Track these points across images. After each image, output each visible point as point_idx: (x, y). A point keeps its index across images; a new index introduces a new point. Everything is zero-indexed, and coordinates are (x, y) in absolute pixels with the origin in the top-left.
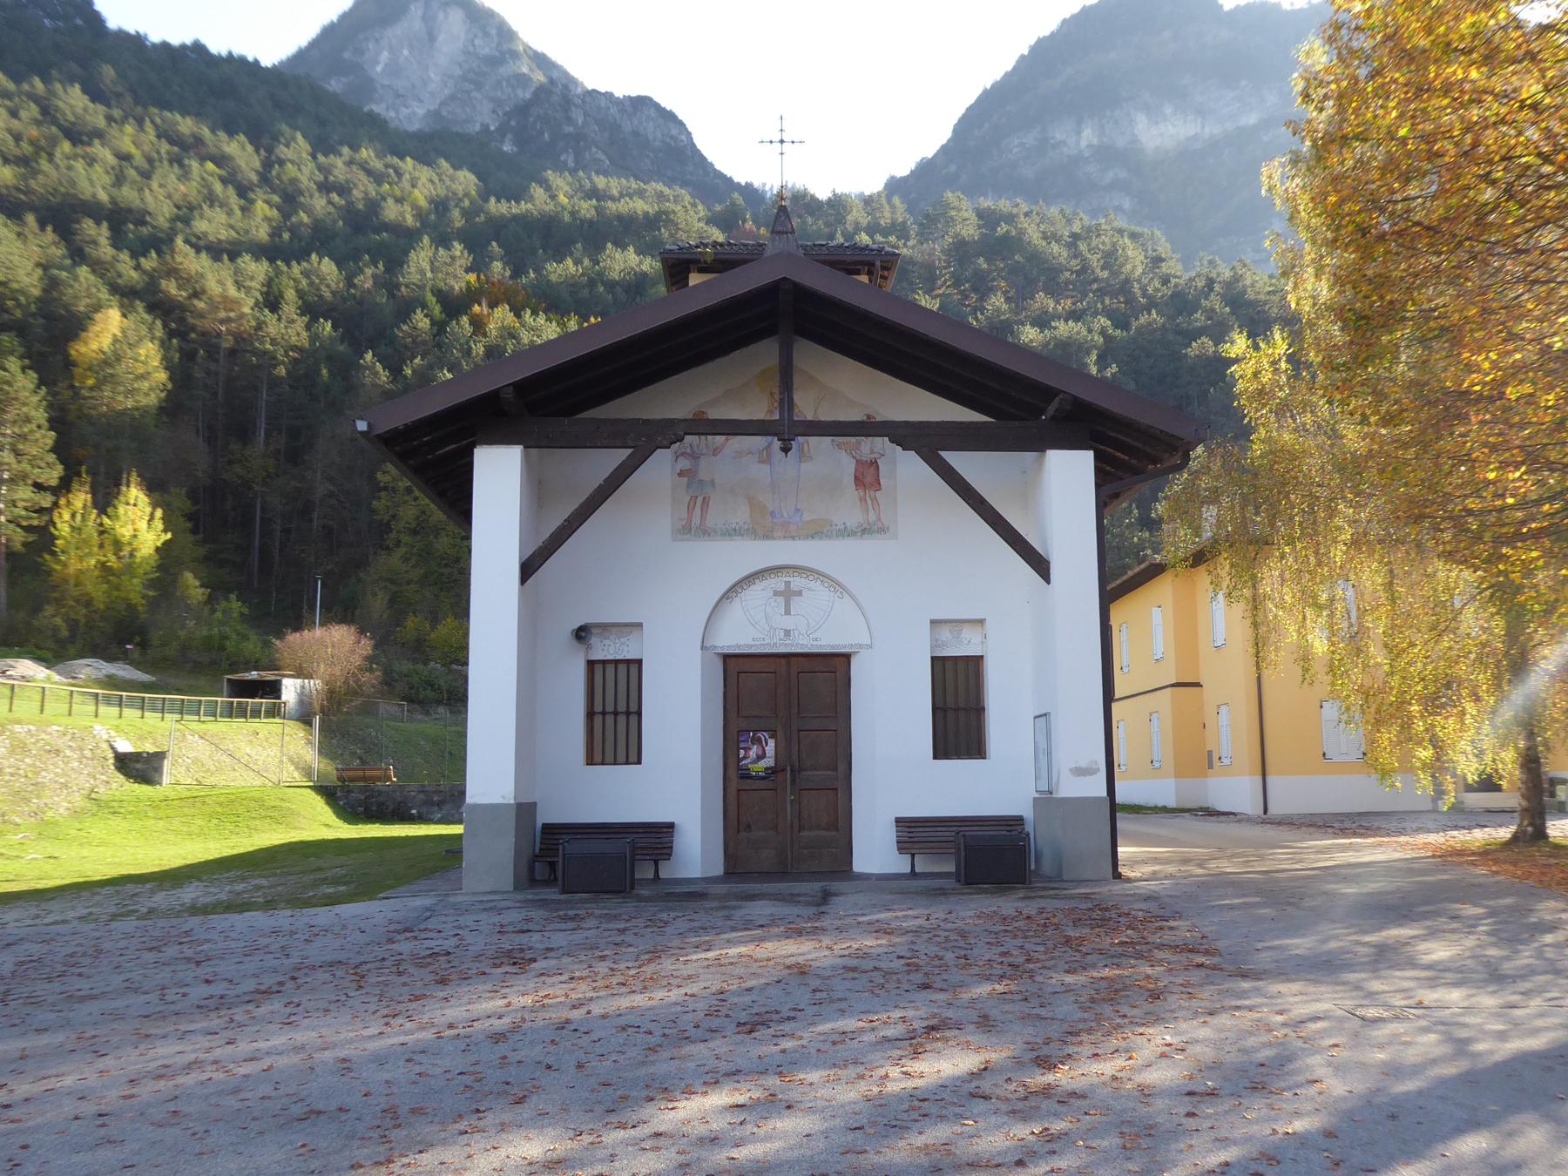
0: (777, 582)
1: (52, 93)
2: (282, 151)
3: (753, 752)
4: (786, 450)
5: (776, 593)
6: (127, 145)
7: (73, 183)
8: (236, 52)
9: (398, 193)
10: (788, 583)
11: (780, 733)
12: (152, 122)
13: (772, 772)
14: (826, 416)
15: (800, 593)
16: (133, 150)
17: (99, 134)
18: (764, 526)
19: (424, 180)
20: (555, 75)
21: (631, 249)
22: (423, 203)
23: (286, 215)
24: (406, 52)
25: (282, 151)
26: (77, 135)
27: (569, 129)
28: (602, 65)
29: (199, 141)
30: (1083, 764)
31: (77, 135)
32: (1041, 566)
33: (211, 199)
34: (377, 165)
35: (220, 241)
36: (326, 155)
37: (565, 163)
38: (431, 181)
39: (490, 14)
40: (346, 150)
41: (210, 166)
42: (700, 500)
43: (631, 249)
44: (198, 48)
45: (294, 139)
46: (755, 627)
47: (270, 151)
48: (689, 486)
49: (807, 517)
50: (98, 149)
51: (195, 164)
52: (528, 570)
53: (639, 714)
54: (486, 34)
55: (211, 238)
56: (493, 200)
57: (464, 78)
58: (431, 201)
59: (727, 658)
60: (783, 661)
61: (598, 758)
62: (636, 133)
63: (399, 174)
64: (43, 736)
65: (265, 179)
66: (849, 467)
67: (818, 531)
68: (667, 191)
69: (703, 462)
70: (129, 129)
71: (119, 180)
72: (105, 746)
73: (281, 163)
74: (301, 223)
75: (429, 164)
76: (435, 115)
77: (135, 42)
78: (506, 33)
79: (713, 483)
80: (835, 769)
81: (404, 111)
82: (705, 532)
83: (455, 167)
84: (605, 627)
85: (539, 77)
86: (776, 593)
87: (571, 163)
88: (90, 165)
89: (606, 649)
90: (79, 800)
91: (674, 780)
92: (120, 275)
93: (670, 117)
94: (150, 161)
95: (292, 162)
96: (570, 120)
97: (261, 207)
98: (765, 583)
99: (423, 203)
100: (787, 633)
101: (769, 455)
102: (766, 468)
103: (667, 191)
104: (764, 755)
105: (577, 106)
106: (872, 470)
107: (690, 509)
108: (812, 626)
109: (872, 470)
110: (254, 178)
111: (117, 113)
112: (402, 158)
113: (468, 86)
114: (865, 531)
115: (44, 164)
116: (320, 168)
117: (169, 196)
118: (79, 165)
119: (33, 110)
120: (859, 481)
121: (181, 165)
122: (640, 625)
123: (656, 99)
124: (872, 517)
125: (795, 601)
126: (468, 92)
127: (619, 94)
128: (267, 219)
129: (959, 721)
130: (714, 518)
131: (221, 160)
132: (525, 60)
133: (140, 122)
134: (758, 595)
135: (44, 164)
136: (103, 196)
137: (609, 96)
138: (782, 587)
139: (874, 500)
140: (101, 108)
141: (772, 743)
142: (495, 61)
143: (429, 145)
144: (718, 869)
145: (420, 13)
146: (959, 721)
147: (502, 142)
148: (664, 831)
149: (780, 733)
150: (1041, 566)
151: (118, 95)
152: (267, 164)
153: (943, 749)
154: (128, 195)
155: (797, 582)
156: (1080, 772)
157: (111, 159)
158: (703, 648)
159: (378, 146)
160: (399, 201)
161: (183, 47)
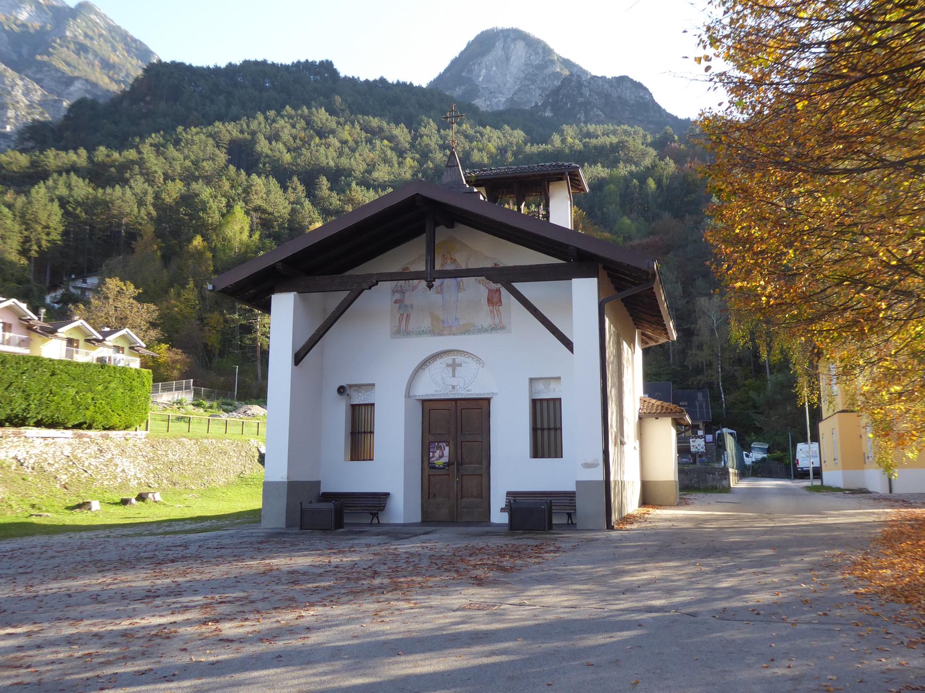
0: (448, 359)
1: (311, 113)
2: (423, 130)
3: (437, 454)
4: (430, 286)
5: (448, 365)
6: (346, 136)
7: (317, 159)
8: (401, 81)
9: (481, 146)
10: (454, 360)
11: (451, 442)
12: (359, 122)
13: (448, 464)
14: (473, 265)
15: (460, 365)
16: (349, 138)
17: (333, 132)
18: (438, 330)
19: (495, 137)
20: (575, 71)
21: (599, 165)
22: (493, 150)
23: (421, 164)
24: (494, 68)
25: (423, 130)
26: (322, 133)
27: (581, 100)
28: (600, 62)
29: (381, 129)
30: (590, 461)
31: (322, 133)
32: (569, 345)
33: (386, 161)
34: (471, 132)
35: (385, 182)
36: (445, 130)
37: (579, 119)
38: (499, 138)
39: (538, 42)
40: (455, 126)
41: (385, 142)
42: (405, 316)
43: (599, 165)
44: (383, 81)
45: (429, 123)
46: (435, 384)
47: (416, 131)
48: (399, 308)
49: (461, 323)
50: (333, 140)
51: (378, 142)
52: (298, 358)
53: (561, 429)
54: (537, 53)
55: (380, 180)
56: (529, 144)
57: (525, 78)
58: (498, 149)
59: (424, 402)
60: (454, 403)
61: (540, 454)
62: (619, 97)
63: (482, 135)
64: (220, 445)
65: (413, 146)
66: (485, 293)
67: (467, 330)
68: (629, 129)
69: (407, 294)
70: (347, 127)
71: (341, 155)
72: (255, 450)
73: (421, 136)
74: (429, 167)
75: (499, 129)
76: (511, 100)
77: (353, 82)
78: (547, 51)
79: (412, 306)
80: (481, 464)
81: (495, 100)
82: (408, 333)
83: (513, 129)
84: (359, 387)
85: (566, 73)
86: (448, 365)
87: (583, 118)
88: (328, 148)
89: (359, 398)
90: (232, 477)
91: (391, 469)
92: (331, 204)
93: (639, 86)
94: (357, 143)
95: (427, 136)
96: (582, 95)
97: (409, 161)
98: (442, 360)
99: (493, 150)
100: (453, 387)
101: (442, 290)
102: (439, 296)
103: (629, 129)
104: (442, 455)
105: (586, 86)
106: (497, 294)
107: (400, 322)
108: (468, 383)
109: (497, 294)
110: (408, 146)
111: (342, 120)
112: (484, 127)
113: (527, 82)
114: (493, 329)
115: (304, 151)
116: (441, 137)
117: (364, 160)
118: (322, 149)
119: (303, 123)
120: (490, 301)
121: (371, 143)
122: (374, 385)
123: (630, 77)
124: (497, 321)
125: (458, 368)
126: (528, 86)
127: (609, 76)
128: (411, 167)
129: (546, 434)
130: (413, 325)
131: (391, 138)
132: (558, 64)
133: (353, 123)
134: (438, 366)
135: (304, 151)
136: (332, 164)
137: (603, 78)
138: (451, 362)
139: (498, 311)
140: (334, 118)
141: (447, 449)
142: (540, 68)
143: (497, 119)
144: (418, 518)
145: (501, 46)
146: (546, 434)
147: (545, 111)
148: (383, 498)
149: (451, 442)
150: (569, 345)
151: (343, 110)
152: (414, 138)
153: (538, 451)
154: (344, 162)
155: (459, 359)
156: (587, 466)
157: (338, 144)
158: (408, 395)
159: (472, 122)
160: (480, 150)
161: (375, 81)
